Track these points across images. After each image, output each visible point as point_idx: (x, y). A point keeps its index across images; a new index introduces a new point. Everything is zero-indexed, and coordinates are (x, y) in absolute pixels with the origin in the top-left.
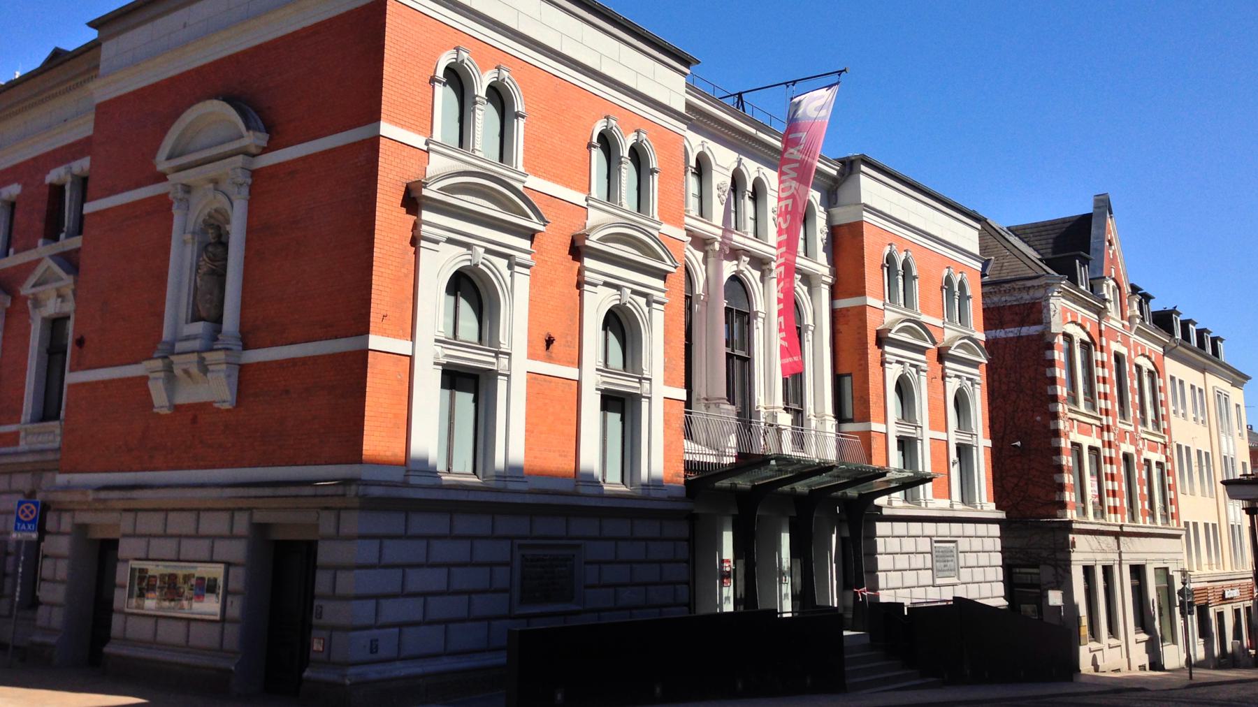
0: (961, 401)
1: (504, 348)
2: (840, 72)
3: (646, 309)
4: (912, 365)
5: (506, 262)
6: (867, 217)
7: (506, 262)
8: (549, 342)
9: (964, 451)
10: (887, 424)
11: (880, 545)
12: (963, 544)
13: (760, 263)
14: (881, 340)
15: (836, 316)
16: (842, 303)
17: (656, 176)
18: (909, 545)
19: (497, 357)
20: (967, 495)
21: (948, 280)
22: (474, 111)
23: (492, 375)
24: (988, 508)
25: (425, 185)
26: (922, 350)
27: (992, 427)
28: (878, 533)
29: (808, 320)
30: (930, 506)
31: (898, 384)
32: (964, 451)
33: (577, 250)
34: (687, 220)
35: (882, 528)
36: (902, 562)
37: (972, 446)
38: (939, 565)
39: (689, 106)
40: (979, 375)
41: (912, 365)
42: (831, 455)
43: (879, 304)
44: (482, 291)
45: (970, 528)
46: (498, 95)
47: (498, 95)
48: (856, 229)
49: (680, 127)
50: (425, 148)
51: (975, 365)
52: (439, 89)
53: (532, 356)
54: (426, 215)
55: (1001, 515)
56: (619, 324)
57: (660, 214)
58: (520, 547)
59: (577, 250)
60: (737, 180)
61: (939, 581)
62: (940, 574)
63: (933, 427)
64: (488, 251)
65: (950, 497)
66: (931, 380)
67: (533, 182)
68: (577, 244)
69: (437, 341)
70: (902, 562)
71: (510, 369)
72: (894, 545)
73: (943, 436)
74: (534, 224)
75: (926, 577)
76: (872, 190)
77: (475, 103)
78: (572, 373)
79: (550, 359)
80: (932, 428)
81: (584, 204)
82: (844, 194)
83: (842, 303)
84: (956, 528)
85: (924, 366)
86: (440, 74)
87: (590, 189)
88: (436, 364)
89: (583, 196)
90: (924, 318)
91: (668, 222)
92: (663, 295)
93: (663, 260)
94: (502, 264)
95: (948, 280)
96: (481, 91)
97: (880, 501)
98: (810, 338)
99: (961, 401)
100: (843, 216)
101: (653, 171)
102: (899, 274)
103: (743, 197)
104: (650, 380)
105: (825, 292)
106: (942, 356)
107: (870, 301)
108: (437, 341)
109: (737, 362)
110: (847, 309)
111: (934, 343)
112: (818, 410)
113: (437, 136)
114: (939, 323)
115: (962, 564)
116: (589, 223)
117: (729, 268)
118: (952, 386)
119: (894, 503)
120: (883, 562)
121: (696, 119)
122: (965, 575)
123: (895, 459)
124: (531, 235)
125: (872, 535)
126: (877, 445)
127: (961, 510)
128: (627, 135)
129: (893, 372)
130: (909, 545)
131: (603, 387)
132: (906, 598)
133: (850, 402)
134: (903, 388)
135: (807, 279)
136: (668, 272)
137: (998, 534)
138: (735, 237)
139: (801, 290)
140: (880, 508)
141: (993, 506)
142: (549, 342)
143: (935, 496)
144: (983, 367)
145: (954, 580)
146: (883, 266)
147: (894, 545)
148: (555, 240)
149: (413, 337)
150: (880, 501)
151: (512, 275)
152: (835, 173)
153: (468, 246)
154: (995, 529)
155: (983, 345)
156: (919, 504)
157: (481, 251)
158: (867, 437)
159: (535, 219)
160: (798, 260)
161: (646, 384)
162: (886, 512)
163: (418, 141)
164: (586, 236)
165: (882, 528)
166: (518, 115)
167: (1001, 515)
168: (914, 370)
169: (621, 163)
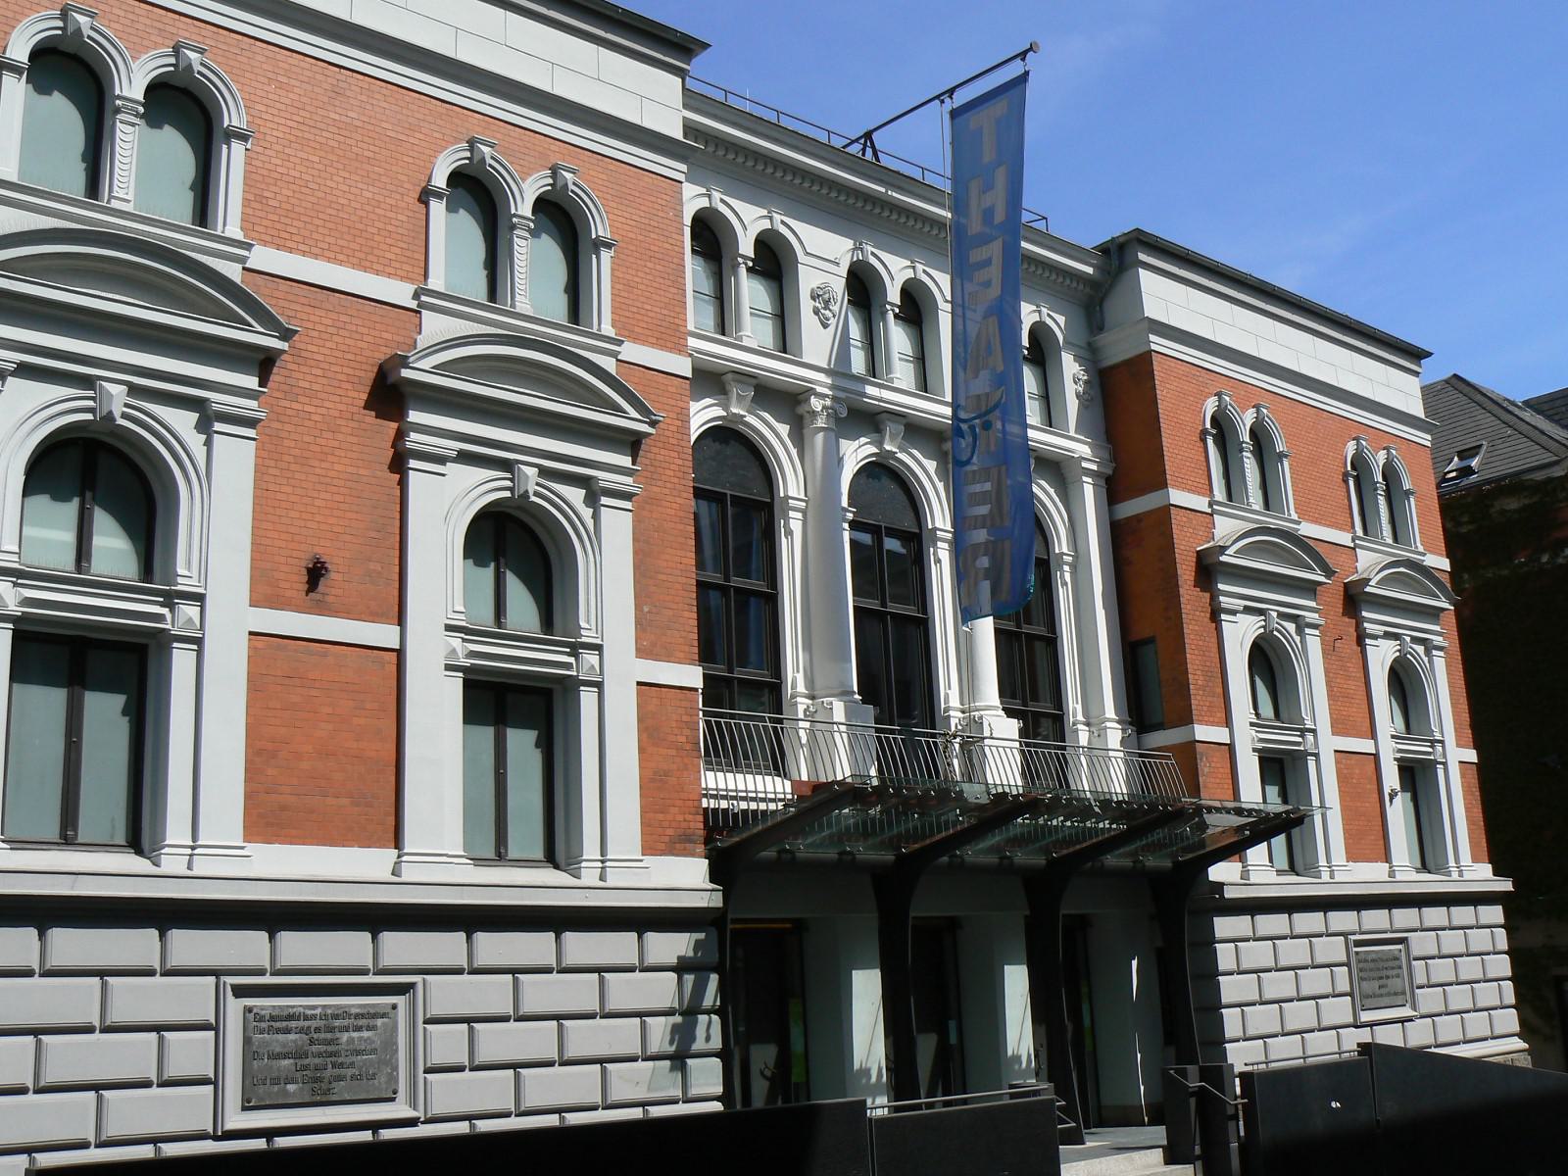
0: (1404, 683)
1: (1309, 725)
2: (1023, 55)
3: (587, 513)
4: (1415, 640)
5: (195, 416)
6: (1158, 343)
7: (195, 416)
8: (316, 574)
9: (1416, 775)
10: (1236, 729)
11: (1225, 956)
12: (444, 995)
13: (787, 401)
14: (1209, 570)
15: (1121, 537)
16: (1130, 508)
17: (606, 256)
18: (1294, 952)
19: (575, 654)
20: (1428, 857)
21: (1360, 464)
22: (511, 241)
23: (569, 687)
24: (1480, 875)
25: (1222, 549)
26: (1309, 589)
27: (1475, 726)
28: (1219, 934)
29: (1062, 545)
30: (1467, 876)
31: (1392, 670)
32: (1416, 775)
33: (390, 394)
34: (692, 342)
35: (1223, 926)
36: (1470, 968)
37: (1305, 754)
38: (1371, 986)
39: (689, 128)
40: (1443, 634)
41: (1415, 640)
42: (1118, 784)
43: (1200, 503)
44: (1271, 654)
45: (1435, 915)
46: (559, 215)
47: (559, 215)
48: (1142, 366)
49: (676, 169)
50: (1209, 511)
51: (1433, 614)
52: (437, 207)
53: (264, 595)
54: (415, 416)
55: (1506, 885)
56: (517, 543)
57: (246, 223)
58: (1358, 944)
59: (390, 394)
60: (862, 287)
61: (1366, 1016)
62: (1368, 1003)
63: (1340, 727)
64: (544, 472)
65: (1387, 859)
66: (1328, 651)
67: (264, 258)
68: (1352, 591)
69: (449, 628)
70: (1470, 968)
71: (1317, 747)
72: (1258, 954)
73: (1365, 746)
74: (1318, 577)
75: (1339, 1010)
76: (1162, 296)
77: (513, 227)
78: (384, 635)
79: (322, 609)
80: (1340, 727)
81: (413, 305)
82: (1114, 308)
83: (1130, 508)
84: (1405, 917)
85: (1438, 640)
86: (440, 181)
87: (426, 276)
88: (448, 667)
89: (1206, 500)
90: (1307, 529)
91: (636, 339)
92: (1316, 616)
93: (617, 409)
94: (575, 495)
95: (1360, 464)
96: (524, 207)
97: (1221, 872)
98: (1068, 577)
99: (1404, 683)
100: (1117, 349)
101: (599, 244)
102: (1242, 446)
103: (736, 274)
104: (598, 648)
105: (1089, 493)
106: (1354, 599)
107: (1177, 496)
108: (449, 628)
109: (1039, 646)
110: (1138, 518)
111: (1329, 572)
112: (1094, 712)
113: (436, 282)
114: (1344, 538)
115: (1420, 979)
116: (423, 341)
117: (856, 453)
118: (1381, 655)
119: (1257, 871)
120: (1231, 988)
121: (703, 151)
122: (1429, 999)
123: (1252, 791)
124: (632, 443)
125: (1209, 941)
126: (1209, 771)
127: (1409, 877)
128: (525, 175)
129: (1240, 633)
130: (1294, 952)
131: (1399, 755)
132: (1285, 1053)
133: (1154, 690)
134: (1268, 661)
135: (1057, 468)
136: (1320, 584)
137: (1502, 921)
138: (870, 390)
139: (1044, 491)
140: (1219, 886)
141: (1485, 870)
142: (316, 574)
143: (1352, 856)
144: (1450, 619)
145: (1406, 1012)
146: (1346, 475)
147: (1258, 954)
148: (328, 381)
149: (401, 620)
150: (1221, 872)
151: (208, 443)
152: (1090, 270)
153: (506, 465)
154: (1495, 914)
155: (1445, 579)
156: (1449, 874)
157: (531, 472)
158: (1188, 751)
159: (634, 414)
160: (1031, 433)
161: (1310, 737)
162: (1230, 893)
163: (400, 292)
164: (403, 361)
165: (1223, 926)
166: (231, 135)
167: (1506, 885)
168: (1420, 649)
169: (1241, 450)
